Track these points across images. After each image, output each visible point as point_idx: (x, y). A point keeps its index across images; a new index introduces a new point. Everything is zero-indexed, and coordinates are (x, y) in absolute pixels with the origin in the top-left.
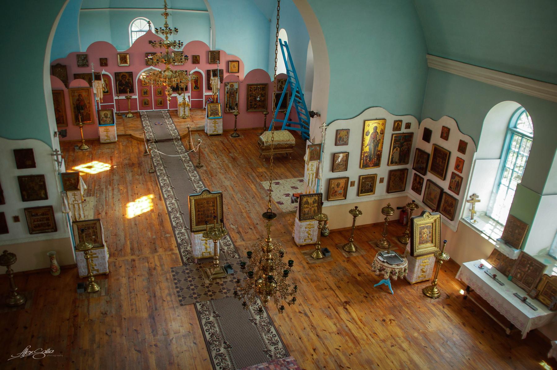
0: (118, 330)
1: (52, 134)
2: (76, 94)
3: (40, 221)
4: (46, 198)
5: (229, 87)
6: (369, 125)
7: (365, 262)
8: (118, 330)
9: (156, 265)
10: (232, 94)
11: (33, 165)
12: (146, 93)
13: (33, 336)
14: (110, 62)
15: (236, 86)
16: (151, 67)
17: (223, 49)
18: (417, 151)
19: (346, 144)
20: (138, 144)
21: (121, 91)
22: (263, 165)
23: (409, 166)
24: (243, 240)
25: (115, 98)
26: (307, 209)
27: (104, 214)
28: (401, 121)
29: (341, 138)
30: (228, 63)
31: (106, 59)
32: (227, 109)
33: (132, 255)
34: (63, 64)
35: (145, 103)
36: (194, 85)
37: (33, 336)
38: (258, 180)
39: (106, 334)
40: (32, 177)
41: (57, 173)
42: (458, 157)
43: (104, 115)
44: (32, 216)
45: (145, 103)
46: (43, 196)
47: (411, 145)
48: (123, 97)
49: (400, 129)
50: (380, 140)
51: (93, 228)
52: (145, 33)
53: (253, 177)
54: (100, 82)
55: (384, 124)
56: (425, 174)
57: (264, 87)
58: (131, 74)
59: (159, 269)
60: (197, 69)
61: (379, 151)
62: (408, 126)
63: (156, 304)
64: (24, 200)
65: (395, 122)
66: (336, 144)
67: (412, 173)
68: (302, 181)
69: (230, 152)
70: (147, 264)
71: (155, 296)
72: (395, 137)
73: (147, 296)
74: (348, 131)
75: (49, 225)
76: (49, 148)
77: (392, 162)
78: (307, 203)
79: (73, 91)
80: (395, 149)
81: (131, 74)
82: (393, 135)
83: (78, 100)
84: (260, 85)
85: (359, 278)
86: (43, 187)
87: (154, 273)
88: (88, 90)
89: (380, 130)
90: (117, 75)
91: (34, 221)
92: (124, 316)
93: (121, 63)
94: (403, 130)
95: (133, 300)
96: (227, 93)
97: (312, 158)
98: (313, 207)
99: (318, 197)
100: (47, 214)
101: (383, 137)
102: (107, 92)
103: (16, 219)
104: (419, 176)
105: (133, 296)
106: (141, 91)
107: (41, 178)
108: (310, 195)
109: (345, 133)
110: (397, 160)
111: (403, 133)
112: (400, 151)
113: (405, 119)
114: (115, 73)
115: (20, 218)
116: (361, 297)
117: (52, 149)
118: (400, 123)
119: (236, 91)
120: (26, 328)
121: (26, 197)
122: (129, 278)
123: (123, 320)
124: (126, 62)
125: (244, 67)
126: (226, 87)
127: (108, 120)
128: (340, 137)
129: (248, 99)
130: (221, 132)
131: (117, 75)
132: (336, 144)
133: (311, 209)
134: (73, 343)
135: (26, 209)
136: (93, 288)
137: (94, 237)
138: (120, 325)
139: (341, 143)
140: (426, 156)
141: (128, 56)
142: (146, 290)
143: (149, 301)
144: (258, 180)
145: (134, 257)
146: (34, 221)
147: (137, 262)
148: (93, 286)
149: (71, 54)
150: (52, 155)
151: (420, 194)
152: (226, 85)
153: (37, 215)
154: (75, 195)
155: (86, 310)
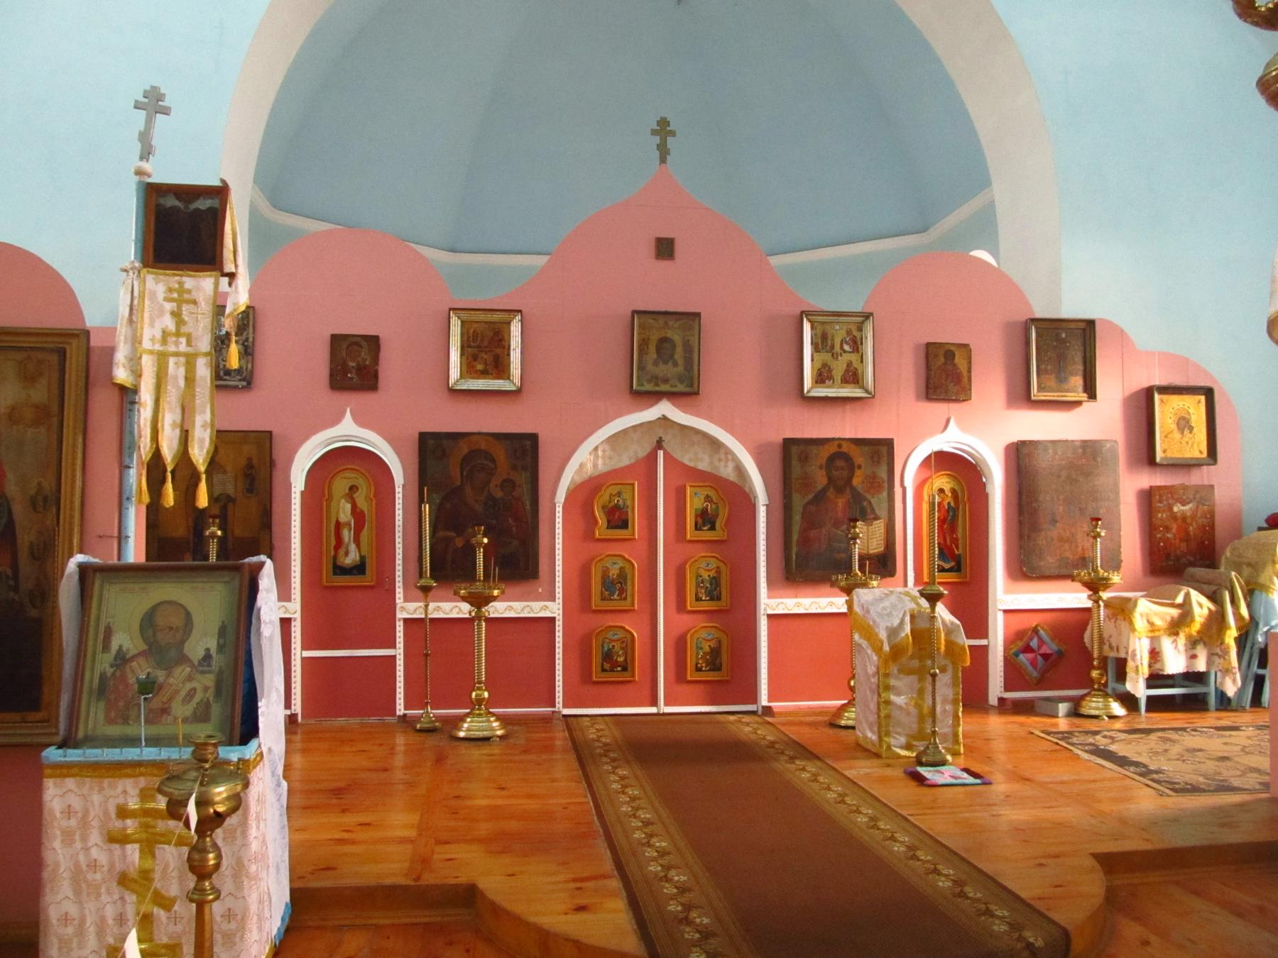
12: (616, 586)
14: (391, 365)
16: (664, 409)
21: (447, 567)
25: (407, 608)
30: (1143, 406)
31: (373, 342)
35: (608, 656)
43: (149, 622)
45: (608, 656)
48: (454, 609)
52: (542, 260)
58: (524, 449)
81: (524, 449)
90: (432, 450)
102: (360, 568)
106: (585, 571)
114: (424, 437)
125: (987, 465)
127: (190, 687)
141: (515, 329)
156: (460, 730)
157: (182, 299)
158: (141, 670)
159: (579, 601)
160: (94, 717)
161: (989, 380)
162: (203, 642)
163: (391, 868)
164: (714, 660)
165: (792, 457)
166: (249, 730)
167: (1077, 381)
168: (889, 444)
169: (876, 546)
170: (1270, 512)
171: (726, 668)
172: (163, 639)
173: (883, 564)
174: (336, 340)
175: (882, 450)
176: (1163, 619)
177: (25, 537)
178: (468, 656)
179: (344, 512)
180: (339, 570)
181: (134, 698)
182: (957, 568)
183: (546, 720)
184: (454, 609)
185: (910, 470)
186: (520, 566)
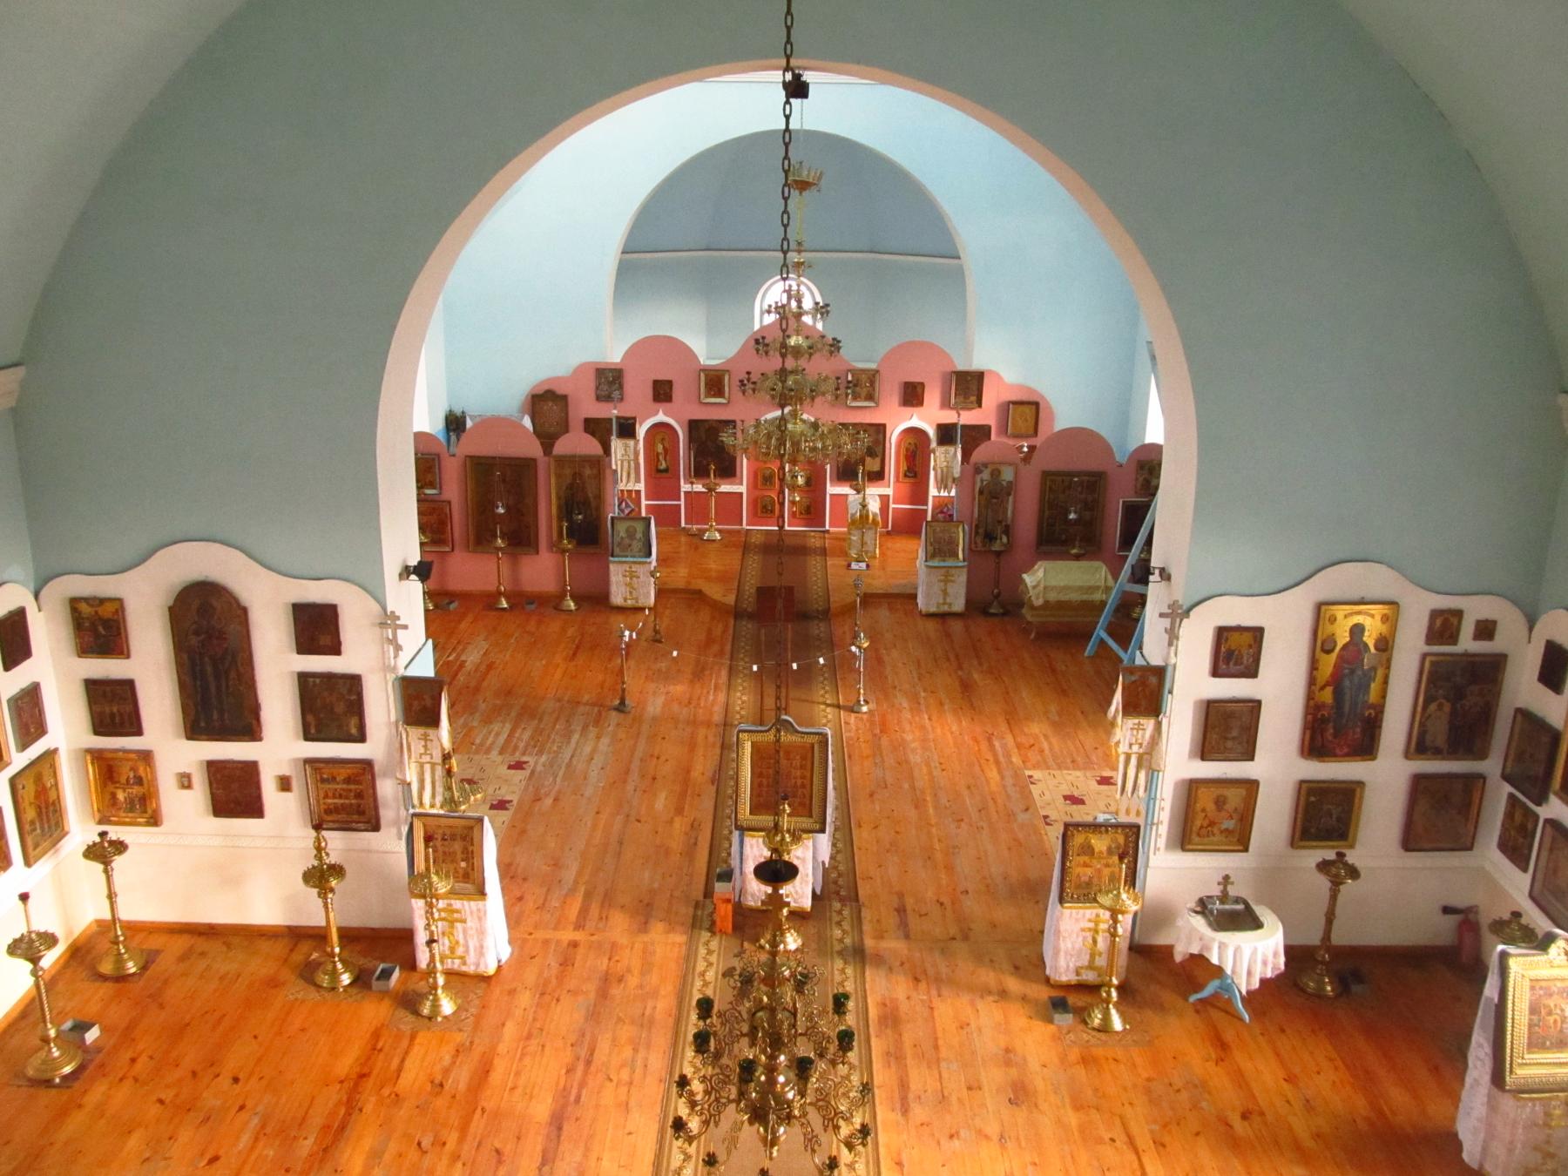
0: (452, 1139)
1: (391, 569)
2: (568, 471)
3: (341, 796)
4: (361, 738)
5: (986, 475)
6: (1333, 620)
7: (1281, 1074)
8: (452, 1139)
9: (629, 970)
11: (335, 649)
13: (242, 1108)
14: (677, 393)
17: (993, 367)
18: (1519, 717)
19: (1251, 672)
20: (713, 618)
21: (700, 472)
22: (1046, 713)
23: (1491, 766)
24: (907, 937)
25: (685, 487)
26: (1089, 871)
27: (549, 801)
28: (1458, 614)
29: (1236, 651)
31: (670, 382)
32: (979, 540)
33: (579, 926)
34: (560, 391)
35: (764, 507)
36: (903, 467)
37: (242, 1108)
38: (1016, 759)
39: (419, 1144)
40: (329, 678)
41: (391, 677)
42: (128, 657)
44: (323, 781)
45: (764, 507)
46: (354, 731)
47: (1497, 695)
49: (1453, 638)
50: (1374, 669)
51: (464, 839)
53: (1004, 746)
54: (631, 443)
55: (1392, 621)
56: (1541, 800)
57: (1094, 483)
59: (633, 981)
60: (915, 422)
61: (1372, 706)
62: (1486, 630)
63: (582, 1085)
64: (308, 737)
65: (1435, 614)
66: (1216, 673)
67: (1499, 795)
68: (1105, 781)
69: (960, 668)
70: (606, 961)
71: (589, 1063)
72: (1433, 663)
73: (567, 1056)
74: (1257, 633)
75: (362, 813)
76: (376, 607)
77: (1419, 746)
78: (1088, 850)
79: (562, 461)
80: (1433, 707)
82: (1424, 656)
83: (571, 486)
84: (1078, 474)
85: (1239, 1126)
86: (356, 707)
87: (616, 991)
88: (599, 465)
89: (1375, 635)
90: (694, 426)
91: (326, 796)
92: (483, 1103)
93: (708, 395)
94: (1467, 643)
95: (527, 1061)
96: (981, 492)
97: (1130, 708)
98: (1107, 865)
99: (1127, 837)
100: (359, 783)
101: (1389, 661)
102: (666, 470)
103: (185, 782)
104: (1524, 804)
105: (532, 1049)
107: (353, 683)
108: (1095, 827)
109: (1247, 638)
110: (1441, 741)
111: (1466, 655)
112: (1454, 713)
113: (1475, 609)
115: (294, 784)
116: (163, 1163)
117: (384, 609)
118: (1454, 621)
119: (1010, 489)
120: (236, 1080)
122: (543, 994)
123: (479, 1111)
124: (720, 394)
127: (637, 545)
128: (1230, 653)
129: (1041, 511)
130: (959, 605)
131: (694, 426)
132: (1216, 673)
133: (1099, 871)
134: (325, 1150)
135: (309, 762)
136: (436, 1006)
137: (463, 864)
138: (464, 1129)
139: (1233, 668)
140: (1545, 739)
142: (573, 1038)
143: (568, 1071)
144: (1016, 759)
145: (578, 936)
146: (326, 796)
147: (581, 950)
148: (436, 999)
149: (582, 368)
150: (383, 625)
151: (1525, 870)
152: (978, 471)
153: (333, 779)
154: (425, 738)
155: (395, 1062)
156: (814, 327)
157: (626, 446)
158: (627, 541)
159: (753, 486)
160: (617, 551)
161: (932, 397)
162: (639, 535)
163: (681, 585)
164: (808, 510)
166: (650, 554)
167: (973, 398)
168: (884, 426)
169: (876, 468)
171: (812, 512)
172: (631, 534)
174: (656, 382)
175: (880, 429)
176: (947, 580)
177: (593, 505)
179: (660, 448)
180: (659, 471)
181: (626, 549)
182: (915, 476)
183: (739, 532)
184: (699, 488)
186: (728, 470)
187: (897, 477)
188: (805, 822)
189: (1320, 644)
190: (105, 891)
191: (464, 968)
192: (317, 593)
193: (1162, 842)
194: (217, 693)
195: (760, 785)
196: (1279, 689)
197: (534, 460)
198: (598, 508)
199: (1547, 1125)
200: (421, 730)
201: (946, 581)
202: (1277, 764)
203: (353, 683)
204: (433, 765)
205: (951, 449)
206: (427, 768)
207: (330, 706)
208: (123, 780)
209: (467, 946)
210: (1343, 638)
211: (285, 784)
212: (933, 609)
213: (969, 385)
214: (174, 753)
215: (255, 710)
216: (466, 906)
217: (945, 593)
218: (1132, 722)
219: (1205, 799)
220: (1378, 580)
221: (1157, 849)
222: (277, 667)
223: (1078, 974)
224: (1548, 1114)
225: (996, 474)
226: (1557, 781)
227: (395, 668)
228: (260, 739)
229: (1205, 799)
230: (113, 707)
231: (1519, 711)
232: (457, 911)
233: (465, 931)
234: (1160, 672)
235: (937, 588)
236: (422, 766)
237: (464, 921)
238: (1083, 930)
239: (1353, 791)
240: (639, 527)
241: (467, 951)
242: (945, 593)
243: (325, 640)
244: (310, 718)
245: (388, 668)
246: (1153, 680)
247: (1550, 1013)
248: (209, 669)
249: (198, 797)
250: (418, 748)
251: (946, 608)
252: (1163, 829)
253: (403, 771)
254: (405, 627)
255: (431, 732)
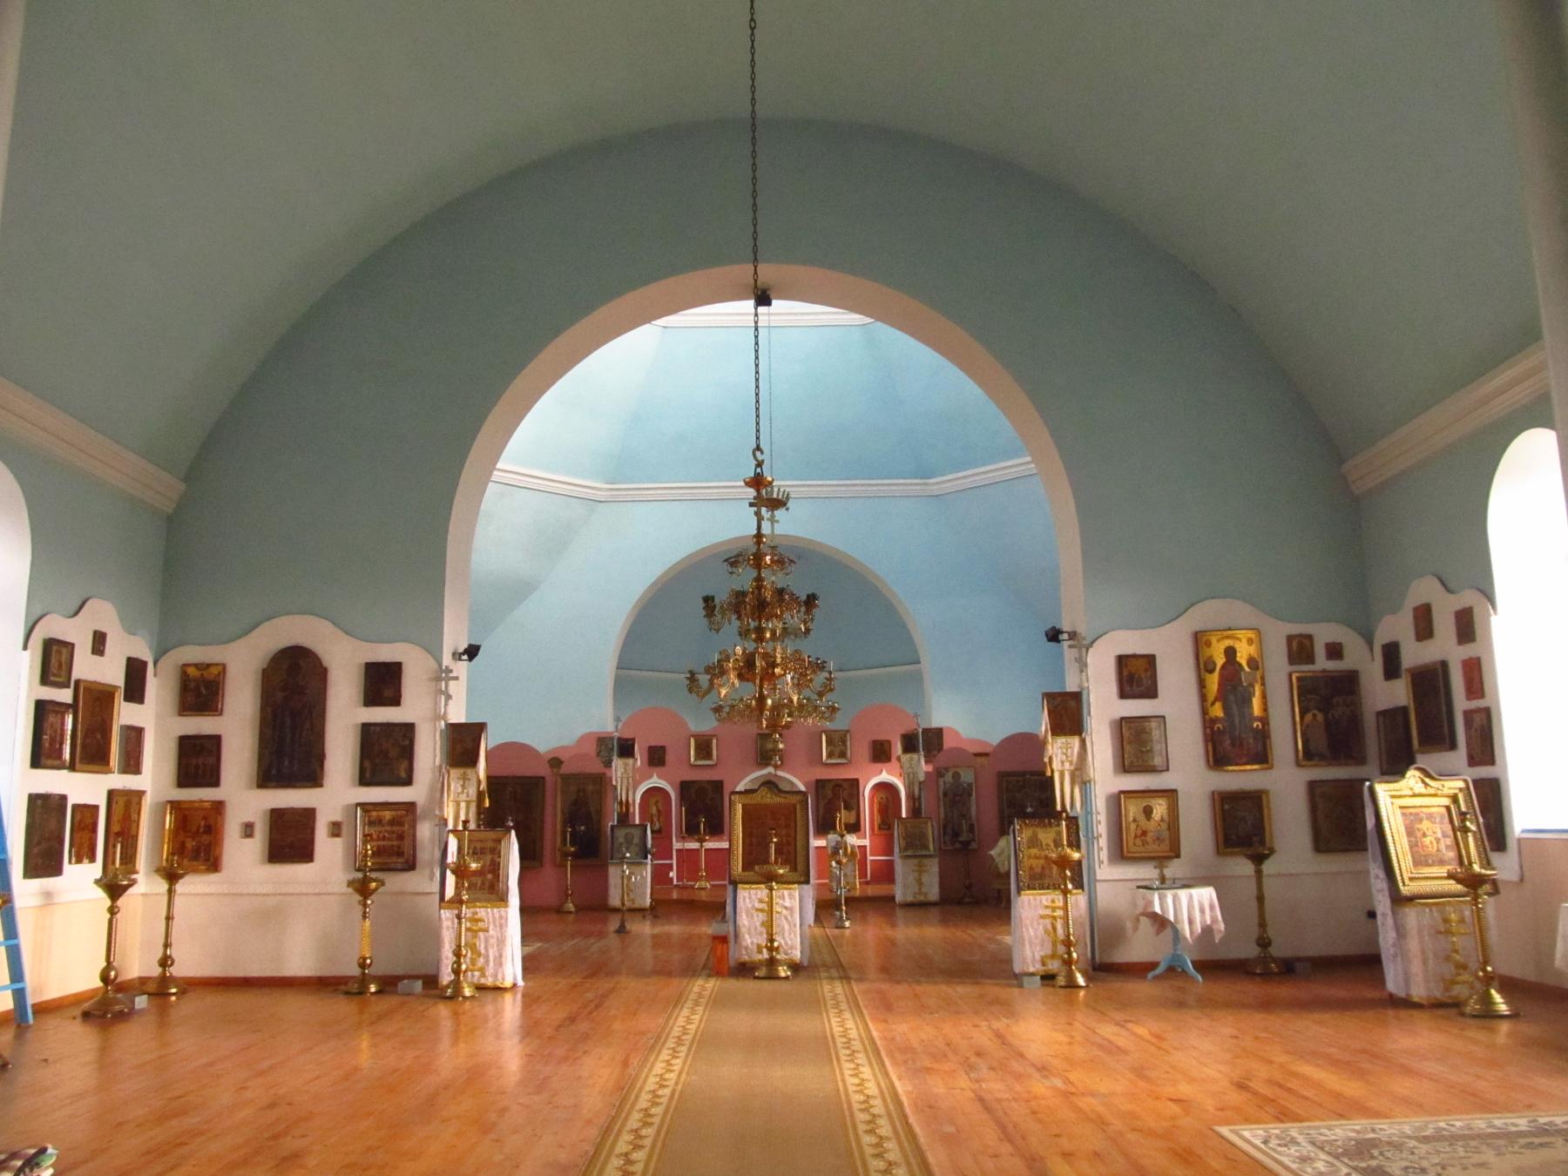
4: (408, 781)
5: (949, 777)
6: (1209, 644)
10: (957, 797)
11: (396, 701)
14: (670, 757)
15: (967, 777)
16: (770, 770)
21: (691, 831)
25: (677, 845)
29: (1136, 676)
31: (663, 748)
46: (403, 775)
48: (694, 845)
49: (1310, 659)
54: (630, 761)
58: (718, 786)
60: (884, 777)
61: (1259, 719)
62: (1335, 651)
72: (1299, 679)
74: (1150, 660)
75: (400, 854)
76: (433, 664)
77: (1309, 755)
80: (1309, 717)
81: (718, 786)
82: (1290, 675)
83: (575, 803)
90: (685, 788)
94: (1322, 663)
96: (945, 795)
112: (1328, 724)
117: (440, 665)
118: (1306, 642)
121: (368, 775)
126: (941, 781)
130: (934, 893)
135: (366, 807)
149: (584, 738)
154: (464, 778)
162: (636, 840)
165: (820, 785)
168: (857, 780)
169: (852, 820)
170: (1202, 762)
173: (855, 828)
175: (855, 784)
176: (920, 870)
178: (699, 860)
179: (654, 810)
184: (694, 845)
185: (867, 791)
187: (872, 828)
188: (795, 876)
189: (1203, 666)
190: (164, 914)
191: (483, 981)
192: (385, 653)
193: (1104, 855)
194: (290, 751)
195: (751, 844)
196: (1177, 705)
197: (543, 778)
198: (599, 822)
199: (1448, 932)
200: (461, 771)
201: (920, 872)
202: (1187, 773)
203: (408, 729)
204: (468, 803)
205: (915, 756)
206: (463, 805)
207: (385, 754)
208: (194, 829)
209: (487, 956)
210: (1220, 660)
211: (336, 829)
212: (910, 899)
213: (928, 741)
214: (244, 800)
215: (321, 758)
216: (486, 913)
217: (920, 884)
218: (1061, 740)
219: (1133, 809)
220: (1240, 611)
221: (1101, 862)
222: (345, 716)
223: (1044, 964)
224: (1446, 921)
225: (956, 776)
226: (1415, 742)
227: (444, 717)
228: (321, 786)
229: (1133, 809)
230: (198, 761)
231: (1379, 714)
232: (481, 920)
233: (487, 940)
234: (1077, 697)
235: (911, 879)
236: (458, 804)
237: (486, 930)
238: (1042, 917)
239: (1260, 798)
240: (636, 833)
241: (487, 962)
242: (920, 884)
243: (388, 693)
244: (367, 764)
245: (438, 717)
246: (1073, 704)
247: (1424, 835)
248: (288, 721)
249: (256, 846)
250: (455, 786)
251: (922, 898)
252: (1103, 842)
253: (441, 809)
254: (457, 678)
255: (469, 771)
